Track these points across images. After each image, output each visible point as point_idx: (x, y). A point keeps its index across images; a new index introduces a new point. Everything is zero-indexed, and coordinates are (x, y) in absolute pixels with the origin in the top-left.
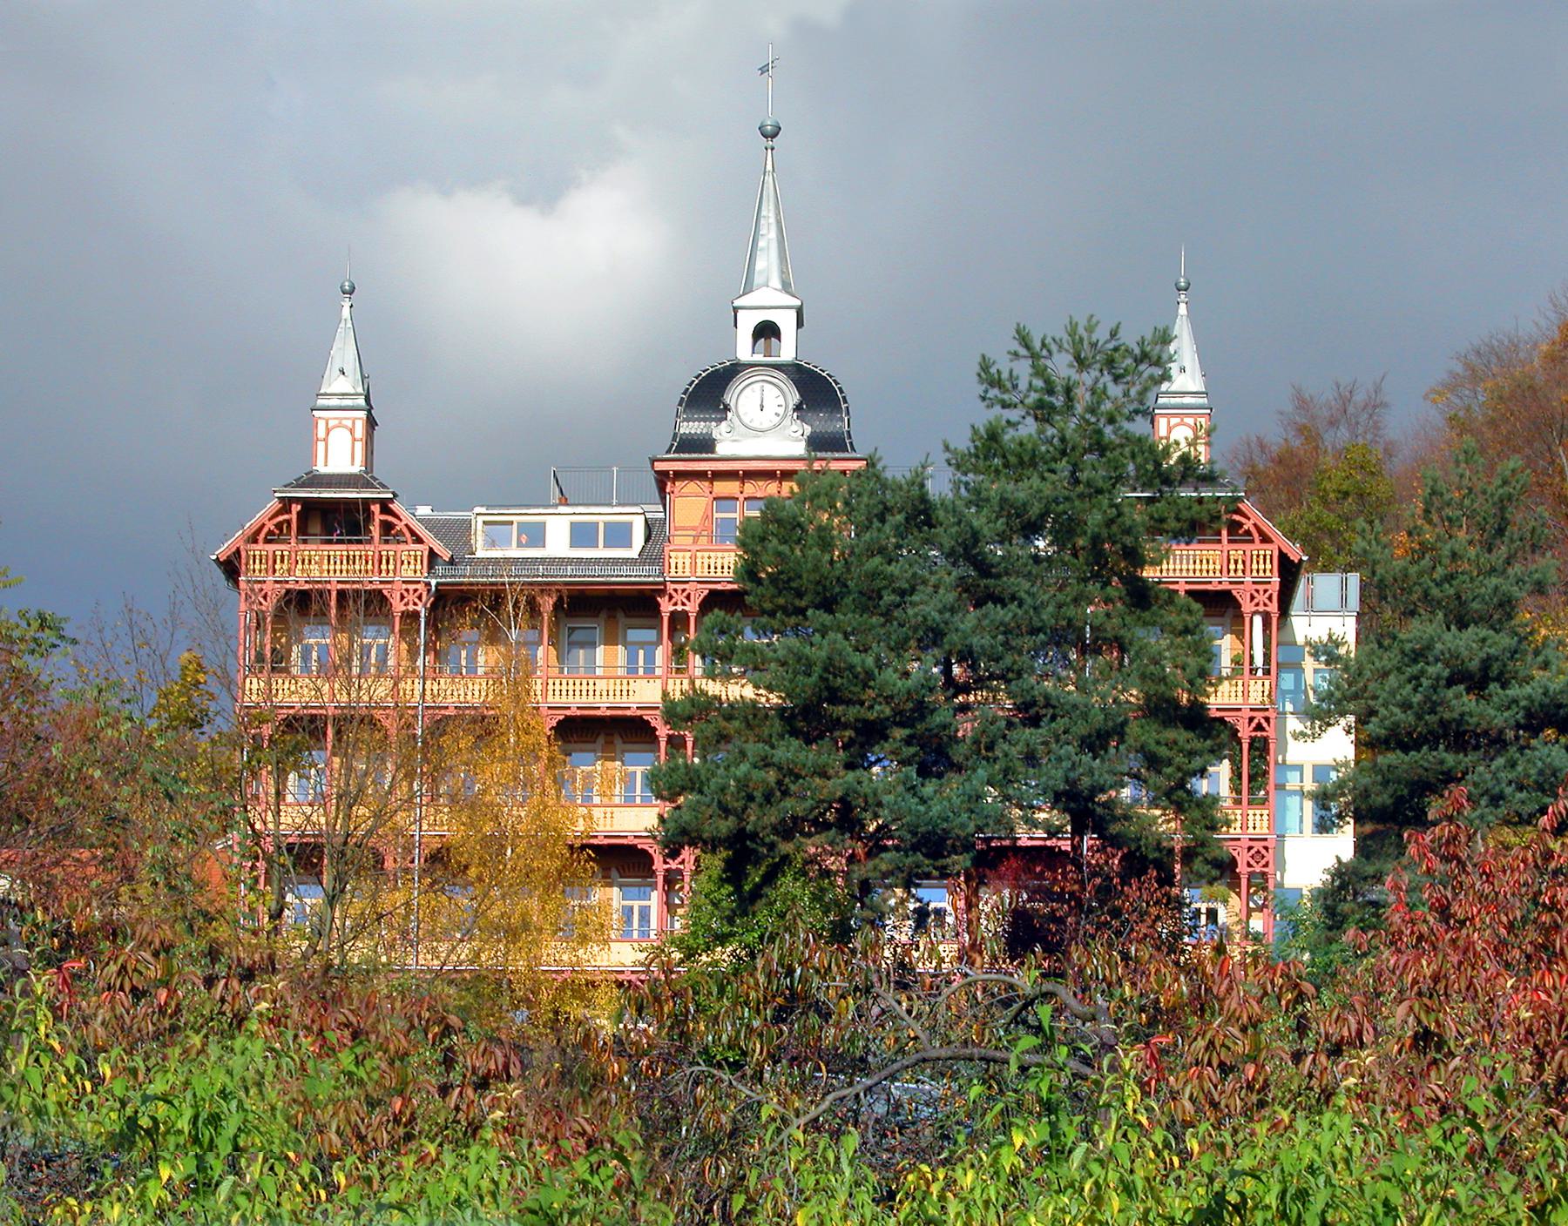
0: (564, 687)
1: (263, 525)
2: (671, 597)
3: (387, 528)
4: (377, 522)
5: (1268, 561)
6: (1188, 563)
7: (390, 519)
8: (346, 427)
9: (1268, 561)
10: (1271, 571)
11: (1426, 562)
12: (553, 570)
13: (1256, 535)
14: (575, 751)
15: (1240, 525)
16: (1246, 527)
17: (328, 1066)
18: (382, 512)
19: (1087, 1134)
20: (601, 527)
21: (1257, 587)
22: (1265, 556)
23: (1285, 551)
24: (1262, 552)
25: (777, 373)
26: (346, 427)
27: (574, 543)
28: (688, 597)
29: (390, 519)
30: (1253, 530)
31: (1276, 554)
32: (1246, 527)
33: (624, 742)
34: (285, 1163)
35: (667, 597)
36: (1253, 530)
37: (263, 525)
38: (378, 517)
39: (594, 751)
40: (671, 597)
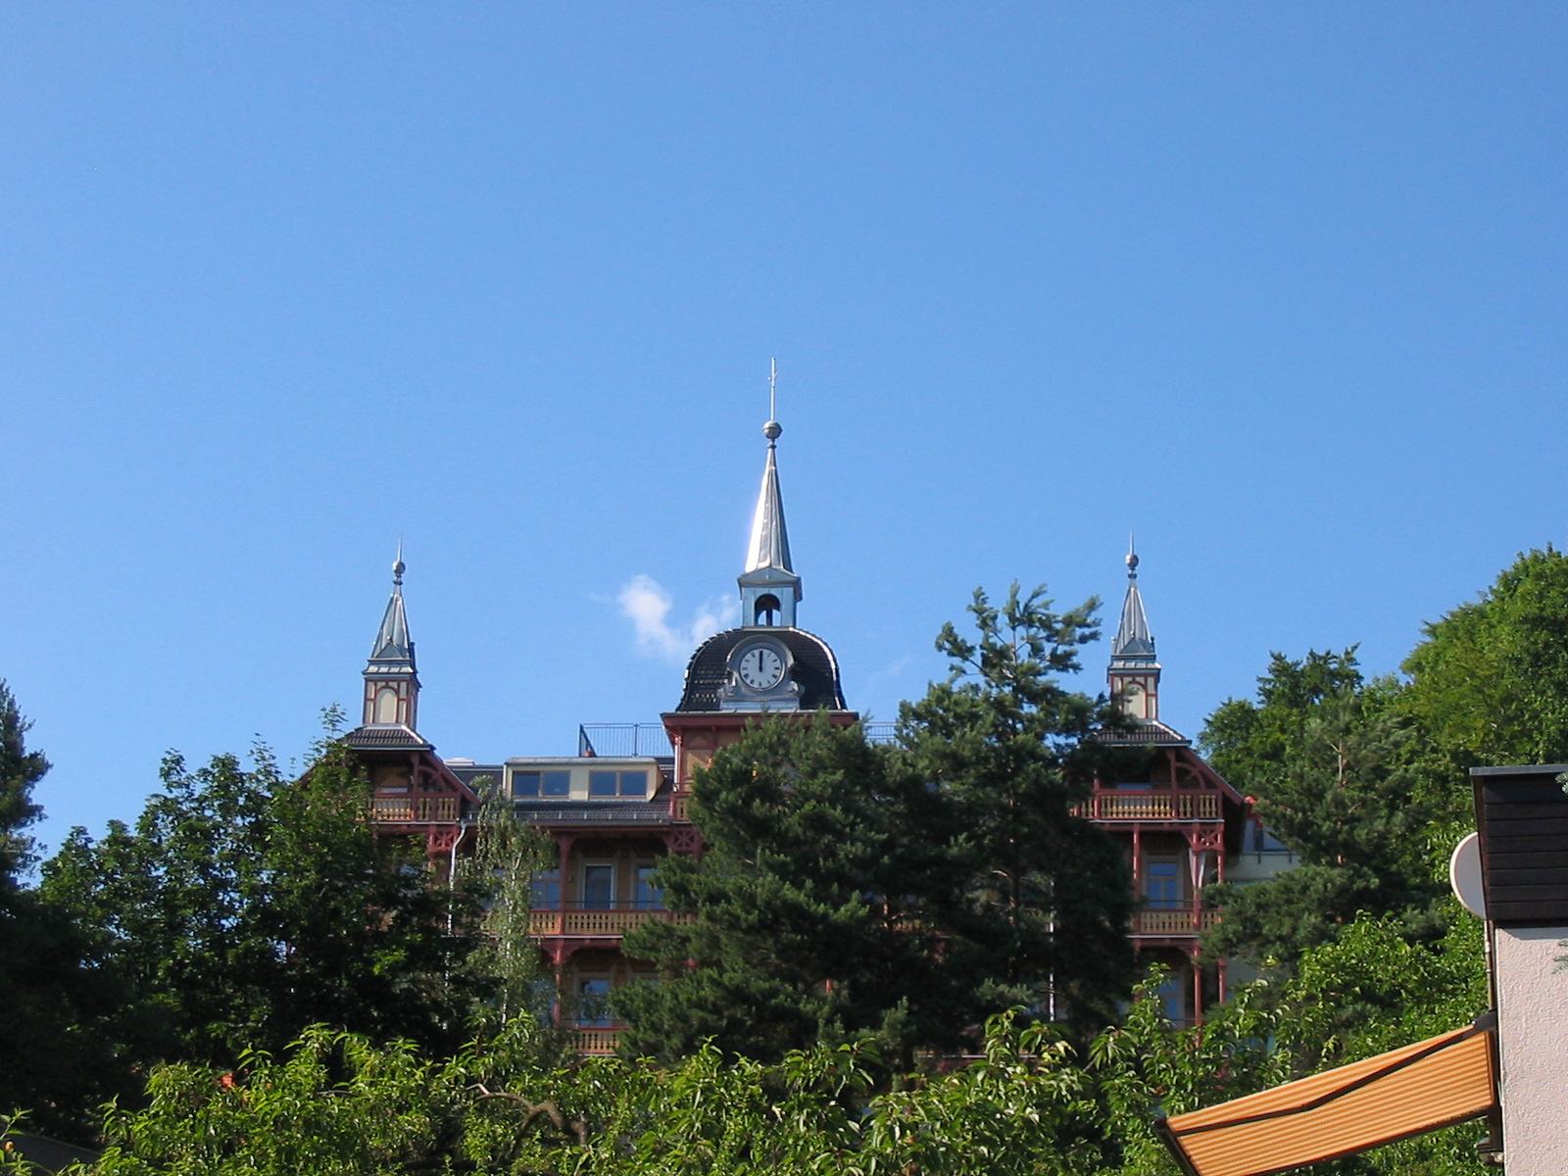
1: (1194, 766)
2: (677, 839)
7: (429, 769)
8: (392, 688)
10: (1217, 813)
11: (626, 1147)
12: (572, 814)
13: (1202, 781)
15: (1188, 772)
16: (1193, 774)
17: (1519, 691)
19: (1390, 920)
20: (618, 774)
22: (1210, 800)
23: (1228, 795)
26: (392, 688)
30: (1199, 776)
32: (1193, 774)
34: (1301, 851)
36: (1199, 776)
37: (1194, 766)
38: (1174, 764)
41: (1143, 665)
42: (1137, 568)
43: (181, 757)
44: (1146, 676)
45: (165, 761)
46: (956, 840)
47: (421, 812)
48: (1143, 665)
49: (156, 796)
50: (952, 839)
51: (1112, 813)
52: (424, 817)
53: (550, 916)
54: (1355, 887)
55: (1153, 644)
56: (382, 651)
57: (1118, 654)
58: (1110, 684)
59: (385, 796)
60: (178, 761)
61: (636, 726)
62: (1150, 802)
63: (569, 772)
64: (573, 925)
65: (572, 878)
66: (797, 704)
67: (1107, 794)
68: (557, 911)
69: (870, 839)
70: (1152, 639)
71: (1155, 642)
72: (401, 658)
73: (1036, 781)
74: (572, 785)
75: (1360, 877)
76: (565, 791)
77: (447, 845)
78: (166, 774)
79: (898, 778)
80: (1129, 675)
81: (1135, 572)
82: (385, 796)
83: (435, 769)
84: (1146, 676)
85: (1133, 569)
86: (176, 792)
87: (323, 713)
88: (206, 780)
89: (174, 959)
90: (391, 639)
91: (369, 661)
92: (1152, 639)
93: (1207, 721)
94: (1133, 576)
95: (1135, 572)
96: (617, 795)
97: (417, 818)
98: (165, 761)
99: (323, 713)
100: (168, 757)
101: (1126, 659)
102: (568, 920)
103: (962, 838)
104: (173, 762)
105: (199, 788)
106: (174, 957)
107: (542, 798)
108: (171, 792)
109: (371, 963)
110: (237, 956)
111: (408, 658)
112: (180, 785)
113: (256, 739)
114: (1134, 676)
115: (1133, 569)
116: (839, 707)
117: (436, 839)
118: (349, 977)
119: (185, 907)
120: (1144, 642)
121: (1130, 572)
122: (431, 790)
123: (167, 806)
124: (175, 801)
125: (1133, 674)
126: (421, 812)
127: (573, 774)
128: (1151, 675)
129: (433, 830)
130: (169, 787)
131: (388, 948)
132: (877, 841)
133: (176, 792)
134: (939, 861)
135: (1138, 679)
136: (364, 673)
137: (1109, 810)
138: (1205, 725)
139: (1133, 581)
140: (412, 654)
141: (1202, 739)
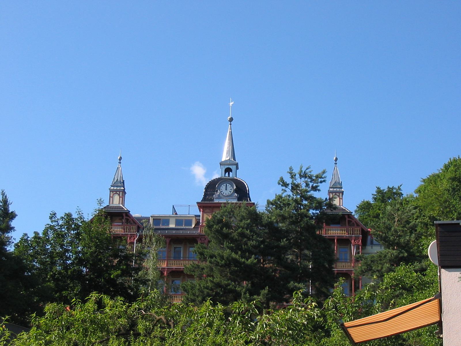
0: (172, 263)
2: (201, 239)
3: (349, 222)
4: (124, 218)
5: (359, 231)
6: (343, 231)
7: (128, 218)
8: (118, 194)
9: (359, 231)
10: (360, 234)
13: (355, 224)
14: (176, 280)
16: (353, 222)
18: (348, 218)
21: (356, 238)
24: (357, 229)
25: (231, 181)
26: (118, 194)
27: (177, 224)
28: (205, 239)
29: (128, 218)
30: (355, 223)
31: (361, 228)
33: (172, 277)
35: (199, 239)
36: (355, 223)
38: (347, 219)
39: (180, 280)
40: (201, 239)
42: (337, 161)
44: (120, 192)
52: (127, 232)
55: (341, 184)
57: (331, 186)
64: (170, 264)
65: (170, 250)
66: (237, 200)
68: (165, 260)
70: (341, 182)
72: (120, 185)
74: (170, 222)
76: (168, 225)
77: (133, 240)
80: (334, 193)
81: (121, 162)
83: (353, 220)
84: (339, 193)
85: (336, 162)
90: (118, 179)
91: (111, 186)
92: (341, 182)
94: (336, 164)
95: (121, 162)
96: (184, 226)
97: (124, 232)
102: (168, 263)
114: (336, 193)
115: (336, 162)
116: (249, 201)
117: (130, 238)
120: (339, 183)
121: (119, 162)
122: (129, 224)
125: (336, 192)
128: (341, 193)
129: (129, 235)
137: (328, 232)
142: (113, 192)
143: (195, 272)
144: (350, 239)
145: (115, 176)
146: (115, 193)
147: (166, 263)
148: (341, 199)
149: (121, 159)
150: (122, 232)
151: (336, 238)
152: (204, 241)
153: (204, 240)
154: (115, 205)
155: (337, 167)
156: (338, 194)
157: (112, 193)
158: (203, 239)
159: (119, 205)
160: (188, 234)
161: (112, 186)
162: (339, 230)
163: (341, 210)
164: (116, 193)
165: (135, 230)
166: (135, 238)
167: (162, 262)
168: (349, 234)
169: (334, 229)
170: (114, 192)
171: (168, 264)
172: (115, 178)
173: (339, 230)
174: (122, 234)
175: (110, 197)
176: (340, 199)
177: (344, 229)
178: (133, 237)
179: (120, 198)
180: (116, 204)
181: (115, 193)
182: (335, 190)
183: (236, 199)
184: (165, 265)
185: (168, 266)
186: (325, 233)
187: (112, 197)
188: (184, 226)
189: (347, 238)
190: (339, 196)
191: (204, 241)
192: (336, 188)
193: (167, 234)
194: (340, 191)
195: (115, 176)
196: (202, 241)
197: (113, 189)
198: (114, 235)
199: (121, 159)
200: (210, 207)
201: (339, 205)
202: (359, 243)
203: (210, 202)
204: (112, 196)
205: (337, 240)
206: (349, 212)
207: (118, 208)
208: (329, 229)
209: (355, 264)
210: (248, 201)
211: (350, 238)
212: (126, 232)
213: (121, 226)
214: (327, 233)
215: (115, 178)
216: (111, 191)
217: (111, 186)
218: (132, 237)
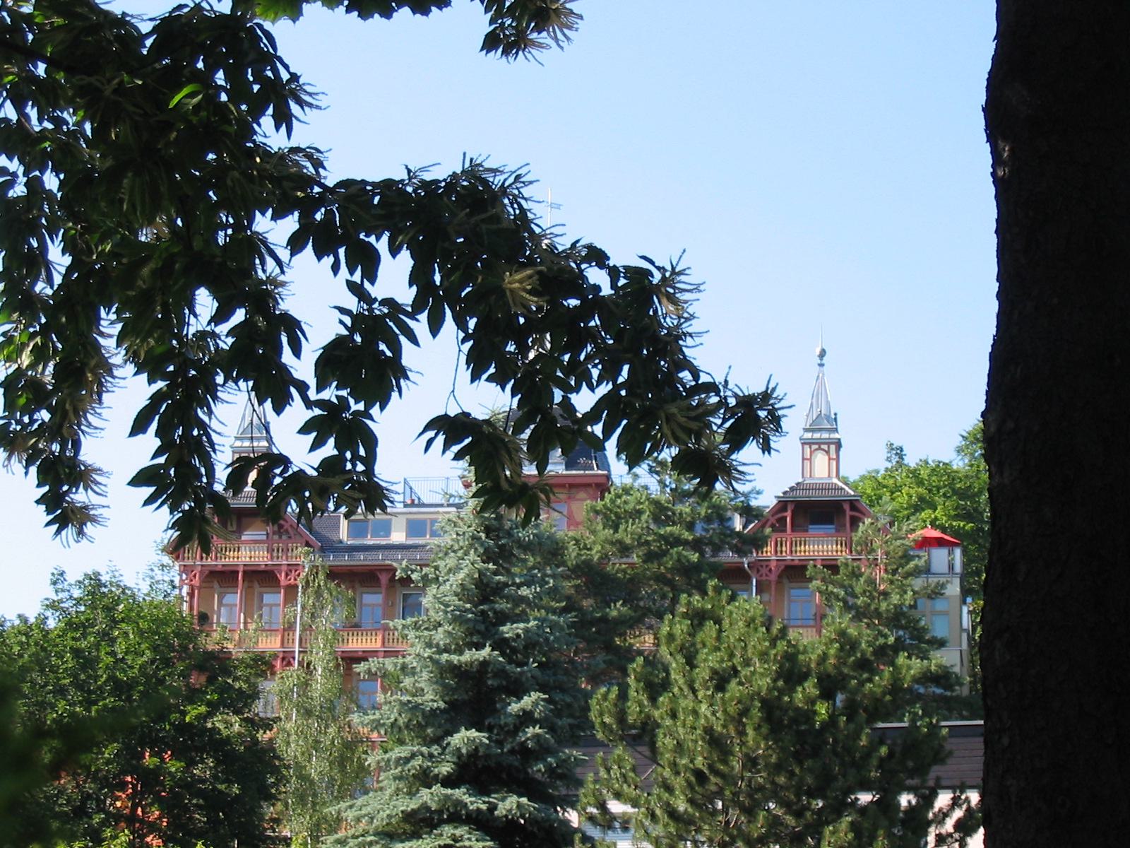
8: (824, 450)
16: (774, 522)
26: (824, 450)
38: (848, 513)
40: (758, 571)
41: (825, 435)
42: (824, 358)
43: (64, 572)
44: (829, 444)
45: (53, 574)
46: (615, 605)
47: (275, 554)
48: (825, 435)
49: (47, 599)
50: (612, 605)
51: (800, 551)
52: (278, 558)
53: (374, 633)
54: (877, 643)
55: (835, 419)
56: (244, 429)
57: (808, 427)
58: (747, 483)
59: (247, 542)
60: (62, 574)
61: (448, 478)
62: (834, 542)
63: (391, 520)
64: (391, 641)
65: (392, 603)
66: (564, 467)
67: (797, 536)
68: (379, 629)
69: (552, 607)
70: (835, 414)
71: (838, 416)
72: (259, 435)
73: (679, 560)
74: (393, 529)
75: (882, 636)
76: (388, 534)
77: (295, 580)
78: (54, 583)
79: (574, 562)
80: (814, 443)
81: (824, 362)
82: (247, 542)
83: (287, 522)
84: (829, 444)
85: (821, 360)
86: (61, 595)
87: (155, 544)
88: (80, 587)
89: (57, 713)
90: (252, 420)
91: (235, 437)
92: (835, 414)
93: (963, 437)
94: (821, 365)
95: (824, 362)
96: (428, 537)
97: (272, 558)
98: (53, 574)
99: (155, 544)
100: (55, 572)
101: (813, 431)
102: (387, 637)
103: (618, 604)
104: (59, 575)
105: (77, 593)
106: (57, 712)
107: (370, 541)
108: (57, 595)
109: (184, 713)
110: (97, 711)
111: (265, 435)
112: (63, 591)
113: (110, 564)
114: (819, 444)
115: (821, 360)
116: (596, 468)
117: (287, 575)
118: (170, 724)
119: (64, 678)
120: (828, 417)
121: (819, 362)
122: (284, 537)
123: (53, 606)
124: (61, 601)
125: (819, 443)
126: (275, 554)
127: (393, 522)
128: (832, 443)
129: (284, 568)
130: (57, 592)
131: (196, 703)
132: (557, 608)
133: (61, 595)
134: (604, 619)
135: (823, 446)
136: (232, 447)
137: (798, 549)
138: (961, 439)
139: (821, 369)
140: (268, 431)
141: (958, 452)
142: (810, 444)
143: (342, 659)
144: (276, 572)
145: (245, 410)
146: (816, 449)
147: (380, 638)
148: (807, 459)
149: (823, 354)
150: (265, 559)
151: (241, 569)
152: (767, 575)
153: (768, 573)
154: (818, 482)
155: (823, 374)
156: (825, 447)
157: (809, 449)
158: (764, 571)
159: (830, 481)
160: (361, 563)
161: (806, 430)
162: (832, 541)
163: (819, 489)
164: (820, 449)
165: (280, 554)
166: (299, 575)
167: (353, 635)
168: (779, 554)
169: (823, 541)
170: (814, 447)
171: (386, 640)
172: (244, 415)
173: (832, 541)
174: (266, 565)
175: (803, 459)
176: (830, 459)
177: (839, 539)
178: (296, 571)
179: (805, 461)
180: (821, 478)
181: (816, 449)
182: (817, 435)
183: (561, 463)
184: (278, 643)
185: (386, 644)
186: (791, 552)
187: (810, 460)
188: (428, 537)
189: (268, 568)
190: (828, 452)
191: (767, 575)
192: (820, 430)
193: (348, 563)
194: (829, 439)
195: (245, 410)
196: (761, 576)
197: (241, 447)
198: (247, 568)
199: (823, 354)
200: (589, 485)
201: (829, 476)
202: (193, 583)
203: (587, 472)
204: (809, 457)
205: (245, 572)
206: (854, 496)
207: (822, 489)
208: (226, 548)
209: (286, 634)
210: (593, 469)
211: (276, 568)
212: (275, 560)
213: (832, 537)
214: (796, 552)
215: (244, 415)
216: (805, 443)
217: (235, 437)
218: (291, 571)
